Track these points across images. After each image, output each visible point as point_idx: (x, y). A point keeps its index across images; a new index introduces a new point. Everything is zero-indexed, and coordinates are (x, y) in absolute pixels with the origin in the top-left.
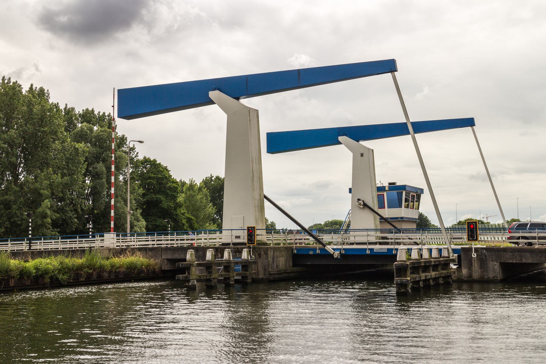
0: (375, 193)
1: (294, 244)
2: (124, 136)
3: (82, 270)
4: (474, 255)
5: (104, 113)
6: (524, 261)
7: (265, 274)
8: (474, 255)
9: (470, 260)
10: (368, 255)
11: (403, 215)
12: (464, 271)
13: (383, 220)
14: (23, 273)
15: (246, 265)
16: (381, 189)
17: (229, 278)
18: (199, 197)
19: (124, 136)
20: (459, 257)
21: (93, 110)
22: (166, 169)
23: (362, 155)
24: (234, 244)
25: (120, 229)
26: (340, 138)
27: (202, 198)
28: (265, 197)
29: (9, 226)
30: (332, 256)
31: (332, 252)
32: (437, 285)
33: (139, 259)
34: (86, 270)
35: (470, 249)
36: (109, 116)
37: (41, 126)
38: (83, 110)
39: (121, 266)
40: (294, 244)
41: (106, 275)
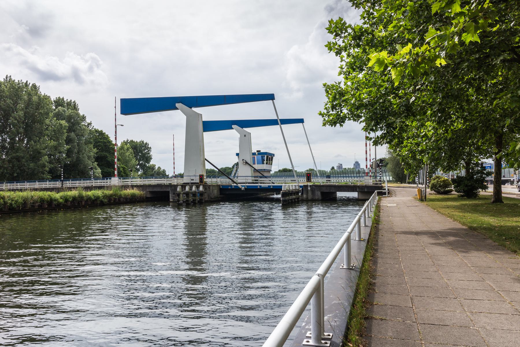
0: (252, 156)
1: (386, 183)
2: (84, 115)
3: (112, 197)
4: (309, 188)
5: (71, 100)
6: (331, 191)
7: (208, 198)
8: (309, 188)
9: (307, 191)
10: (272, 189)
11: (265, 168)
12: (305, 196)
13: (256, 170)
14: (89, 198)
15: (201, 194)
16: (254, 154)
17: (196, 200)
18: (127, 154)
19: (84, 115)
20: (302, 189)
21: (63, 98)
22: (107, 136)
23: (245, 136)
24: (191, 183)
25: (124, 174)
26: (177, 105)
27: (129, 155)
28: (206, 159)
29: (20, 172)
30: (241, 189)
31: (241, 187)
32: (292, 202)
33: (136, 191)
34: (114, 197)
35: (307, 186)
36: (74, 102)
37: (37, 109)
38: (56, 98)
39: (128, 195)
40: (386, 183)
41: (122, 199)
